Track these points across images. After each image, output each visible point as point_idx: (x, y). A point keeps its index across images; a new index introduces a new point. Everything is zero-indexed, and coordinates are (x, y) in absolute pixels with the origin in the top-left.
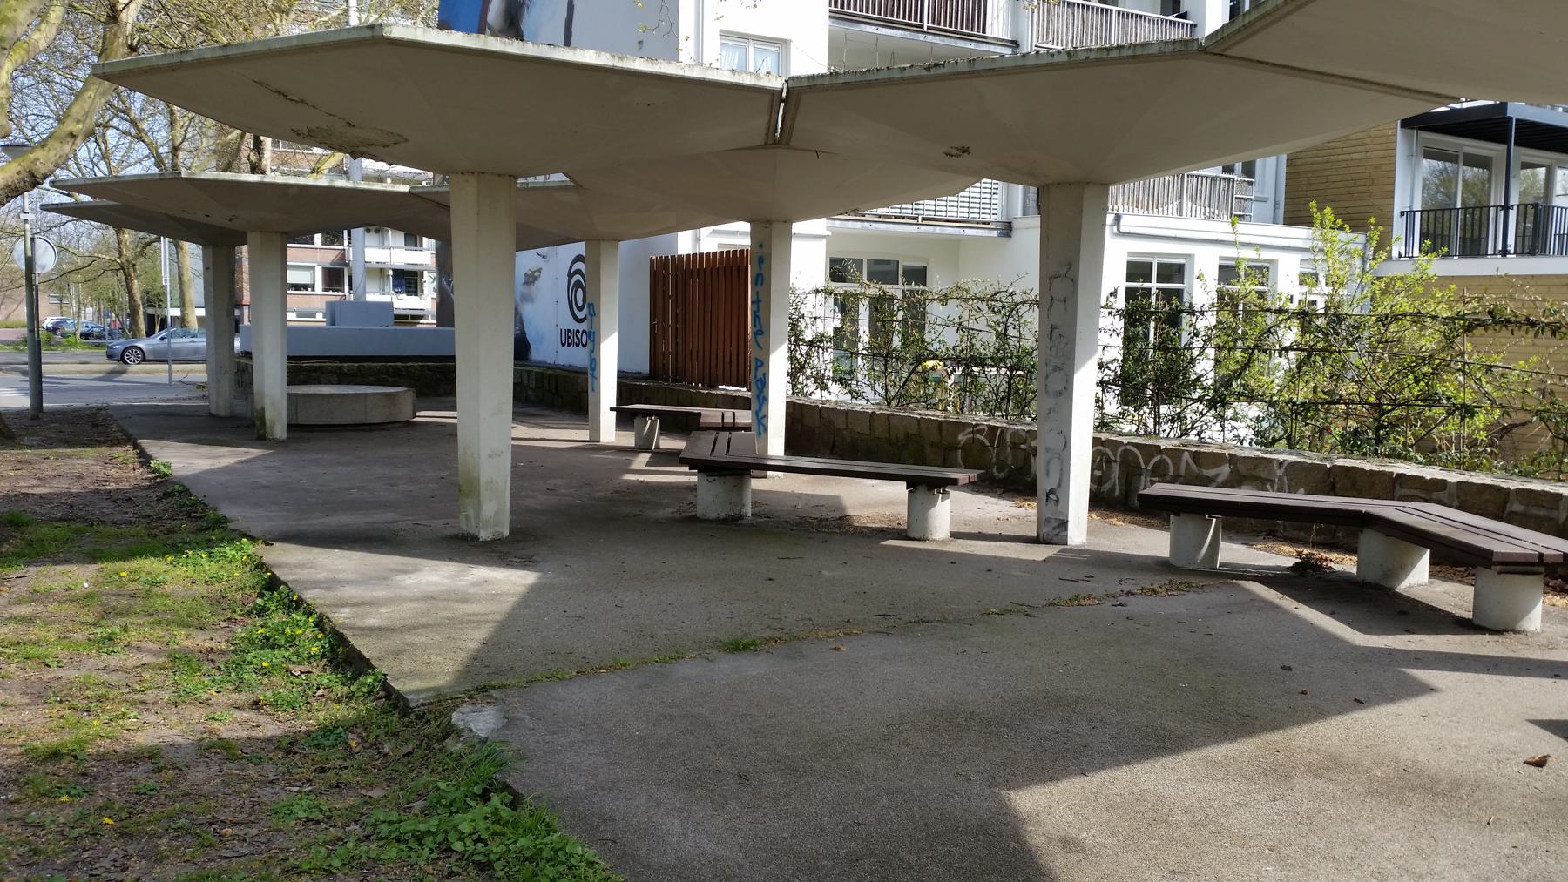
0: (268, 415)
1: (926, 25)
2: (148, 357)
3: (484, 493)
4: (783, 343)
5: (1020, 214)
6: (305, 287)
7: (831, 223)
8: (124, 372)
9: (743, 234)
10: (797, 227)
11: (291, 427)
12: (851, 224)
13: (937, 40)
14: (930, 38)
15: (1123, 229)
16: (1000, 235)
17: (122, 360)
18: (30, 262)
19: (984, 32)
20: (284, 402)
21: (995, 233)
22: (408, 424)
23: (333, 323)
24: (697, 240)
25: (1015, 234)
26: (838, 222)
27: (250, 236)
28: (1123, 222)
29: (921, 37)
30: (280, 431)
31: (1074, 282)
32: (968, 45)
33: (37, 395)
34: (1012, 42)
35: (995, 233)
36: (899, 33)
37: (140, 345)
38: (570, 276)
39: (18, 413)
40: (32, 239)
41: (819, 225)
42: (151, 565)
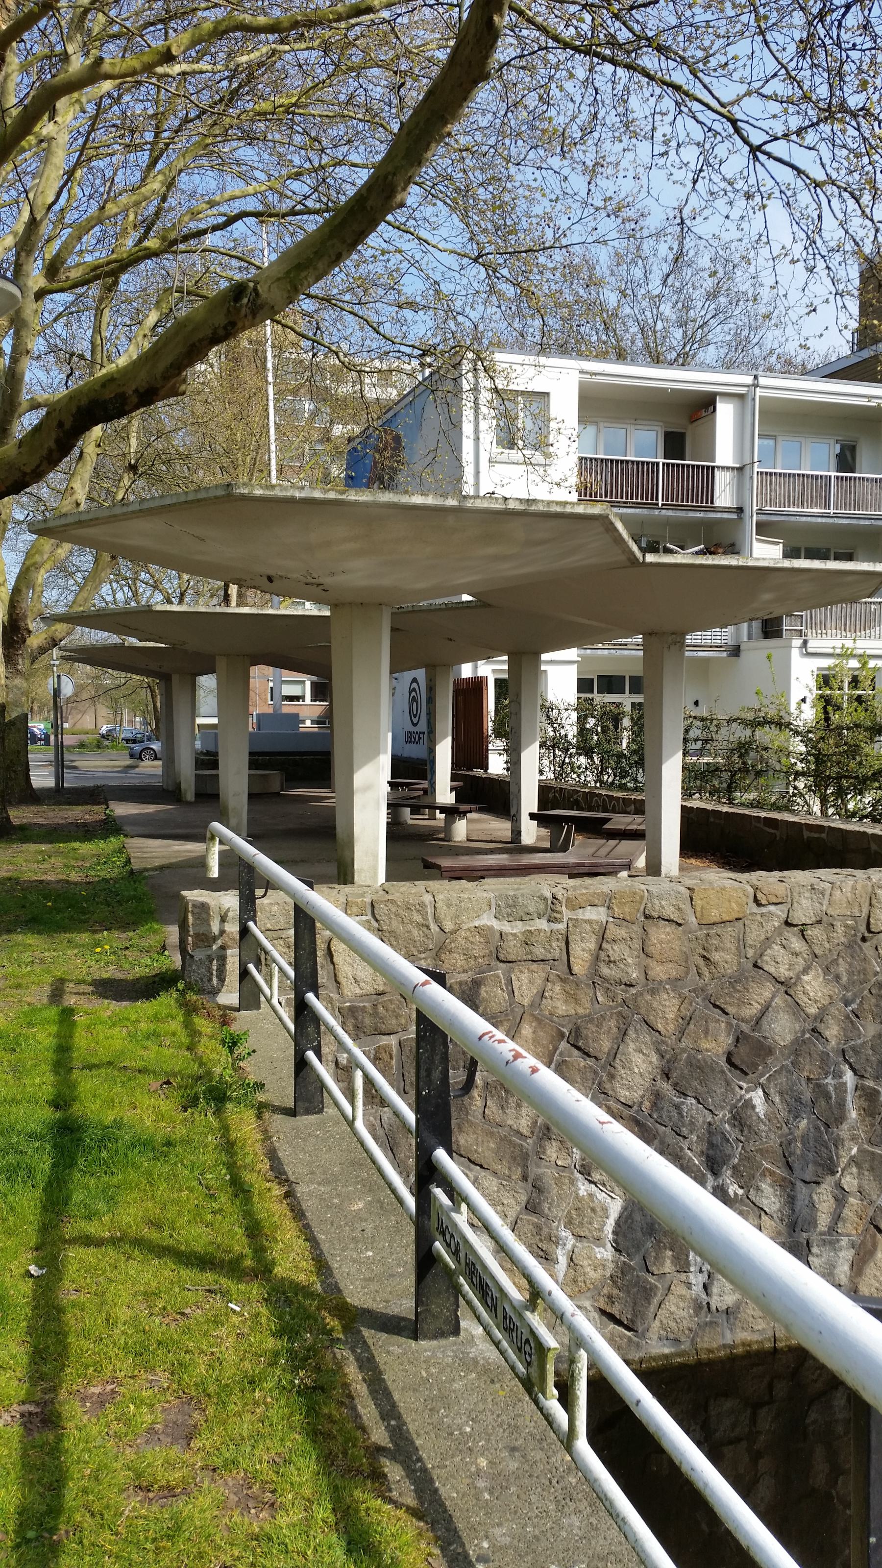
0: (183, 786)
1: (660, 502)
2: (159, 756)
3: (231, 814)
4: (445, 737)
5: (745, 639)
6: (297, 698)
7: (582, 652)
8: (137, 767)
9: (503, 662)
10: (545, 657)
11: (198, 795)
12: (599, 652)
13: (670, 513)
14: (664, 512)
15: (810, 650)
16: (729, 656)
17: (140, 758)
18: (57, 693)
19: (712, 503)
20: (193, 778)
21: (725, 654)
22: (278, 794)
23: (259, 729)
24: (476, 668)
25: (742, 654)
26: (589, 651)
27: (221, 663)
28: (809, 645)
29: (656, 512)
30: (190, 796)
31: (520, 704)
32: (698, 515)
33: (59, 778)
34: (737, 508)
35: (725, 654)
36: (638, 511)
37: (153, 747)
38: (410, 693)
39: (48, 790)
40: (59, 676)
41: (572, 654)
42: (76, 845)
